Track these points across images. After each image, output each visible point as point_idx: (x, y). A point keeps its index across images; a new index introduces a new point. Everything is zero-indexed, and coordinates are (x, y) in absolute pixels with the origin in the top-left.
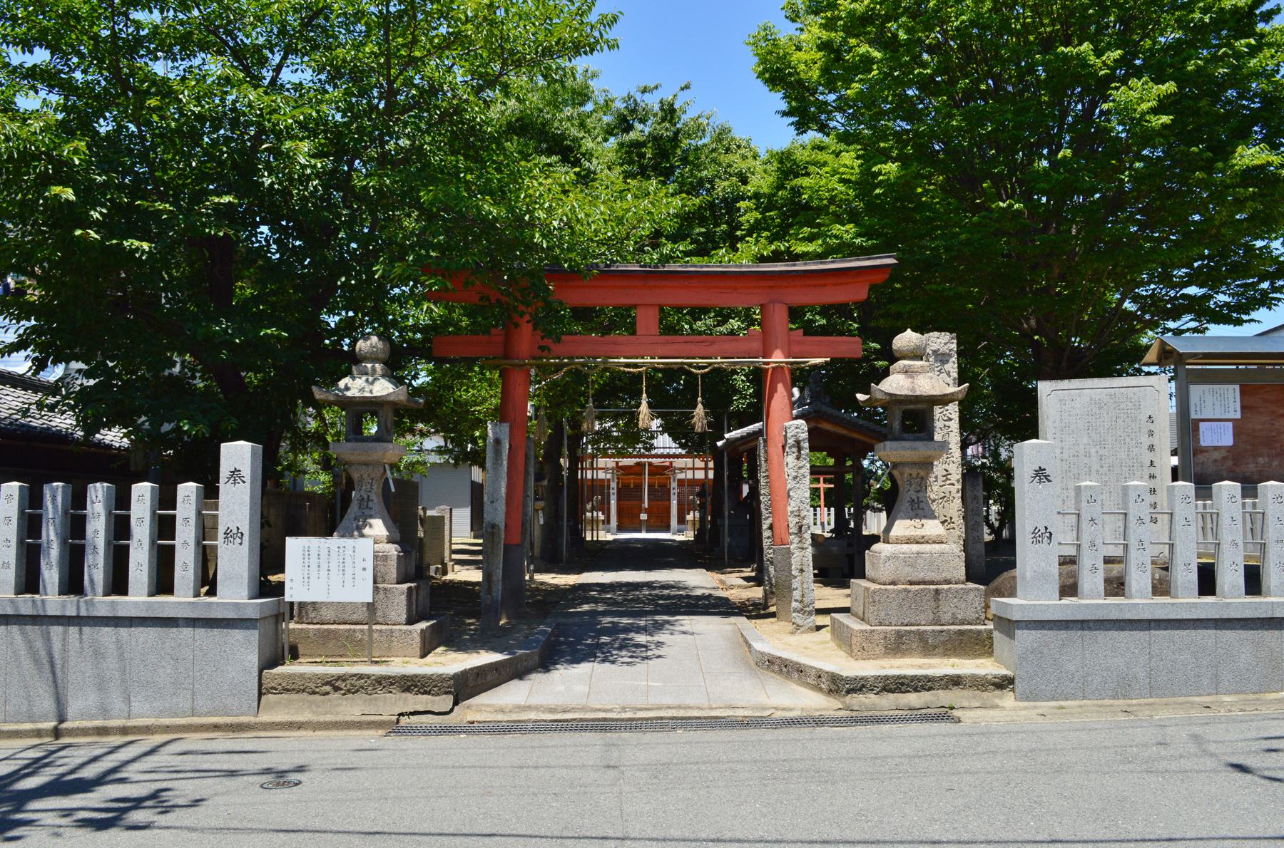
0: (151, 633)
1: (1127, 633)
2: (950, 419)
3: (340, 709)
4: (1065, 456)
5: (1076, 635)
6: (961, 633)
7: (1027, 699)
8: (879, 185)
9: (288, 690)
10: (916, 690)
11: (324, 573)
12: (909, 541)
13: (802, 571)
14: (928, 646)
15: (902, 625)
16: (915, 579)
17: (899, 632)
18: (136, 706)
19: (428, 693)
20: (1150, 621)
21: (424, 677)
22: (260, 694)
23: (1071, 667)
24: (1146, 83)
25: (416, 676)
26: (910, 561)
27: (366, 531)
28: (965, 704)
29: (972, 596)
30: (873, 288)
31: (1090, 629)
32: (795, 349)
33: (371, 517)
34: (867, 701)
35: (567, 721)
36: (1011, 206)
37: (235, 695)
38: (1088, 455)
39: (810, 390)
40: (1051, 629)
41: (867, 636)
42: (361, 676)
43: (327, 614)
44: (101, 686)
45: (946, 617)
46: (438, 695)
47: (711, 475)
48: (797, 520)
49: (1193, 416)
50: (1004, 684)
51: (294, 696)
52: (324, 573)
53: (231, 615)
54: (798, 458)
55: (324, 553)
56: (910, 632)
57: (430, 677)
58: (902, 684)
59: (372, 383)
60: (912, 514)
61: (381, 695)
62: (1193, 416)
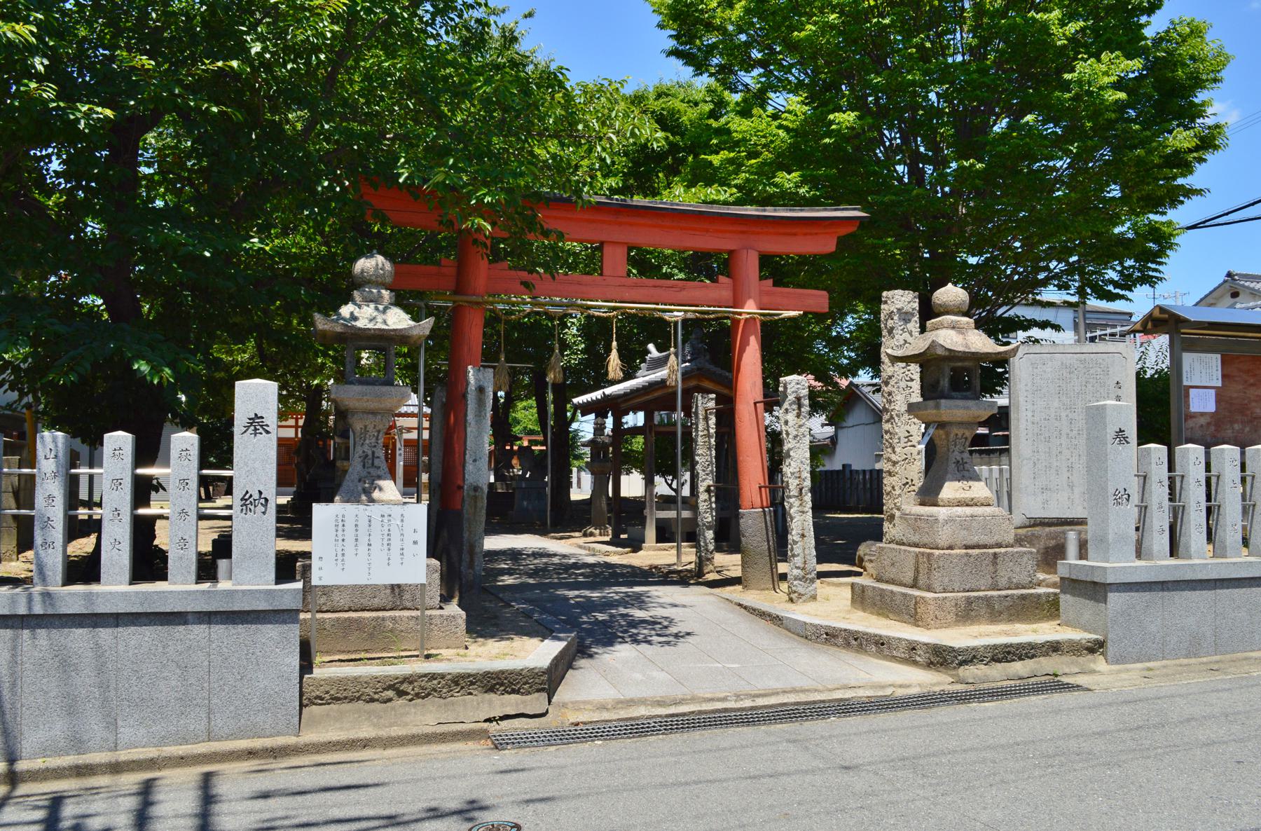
0: (148, 634)
1: (1198, 592)
2: (912, 380)
3: (407, 719)
4: (1036, 419)
5: (1157, 596)
6: (1023, 597)
7: (1117, 662)
8: (829, 134)
9: (338, 699)
10: (1021, 659)
11: (363, 548)
12: (961, 503)
13: (803, 536)
14: (996, 612)
15: (965, 591)
16: (970, 543)
17: (968, 598)
18: (126, 733)
19: (517, 692)
20: (1216, 580)
21: (511, 672)
22: (301, 706)
23: (1153, 628)
24: (1117, 57)
25: (502, 672)
26: (966, 524)
27: (376, 494)
28: (1067, 671)
29: (1025, 559)
30: (842, 242)
31: (1168, 590)
32: (765, 299)
33: (380, 478)
34: (979, 672)
35: (684, 714)
36: (972, 165)
37: (268, 710)
38: (1058, 418)
39: (692, 346)
40: (1137, 591)
41: (940, 604)
42: (433, 676)
43: (341, 600)
44: (71, 709)
45: (1003, 582)
46: (529, 693)
47: (426, 435)
48: (797, 482)
49: (1185, 383)
50: (1096, 648)
51: (346, 706)
52: (363, 548)
53: (262, 606)
54: (798, 416)
55: (363, 523)
56: (978, 598)
57: (519, 673)
58: (1009, 653)
59: (384, 311)
60: (959, 475)
61: (459, 698)
62: (1185, 383)
